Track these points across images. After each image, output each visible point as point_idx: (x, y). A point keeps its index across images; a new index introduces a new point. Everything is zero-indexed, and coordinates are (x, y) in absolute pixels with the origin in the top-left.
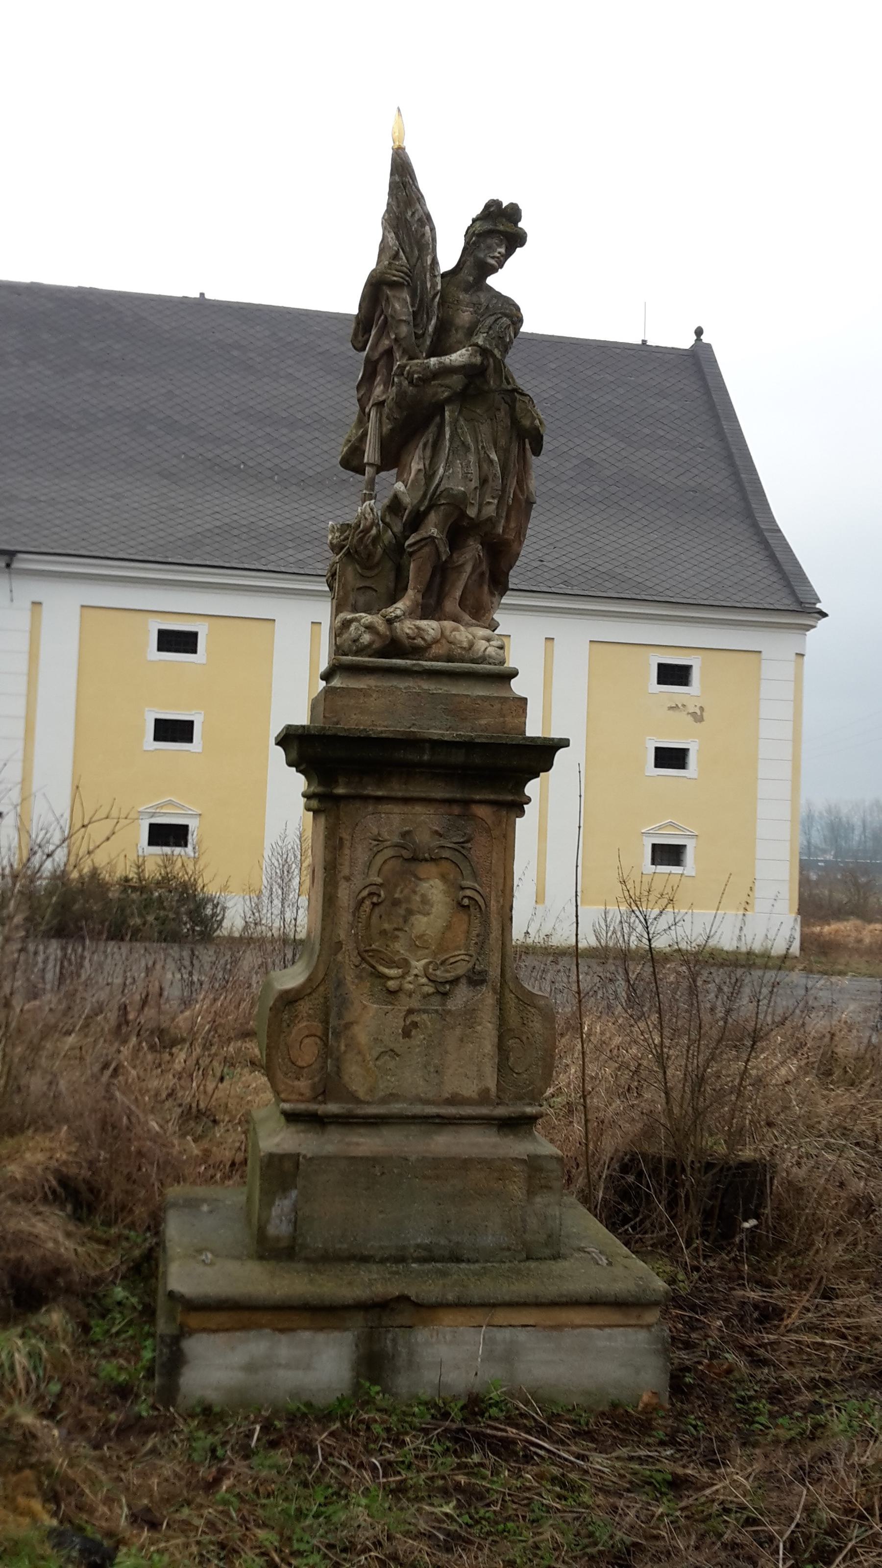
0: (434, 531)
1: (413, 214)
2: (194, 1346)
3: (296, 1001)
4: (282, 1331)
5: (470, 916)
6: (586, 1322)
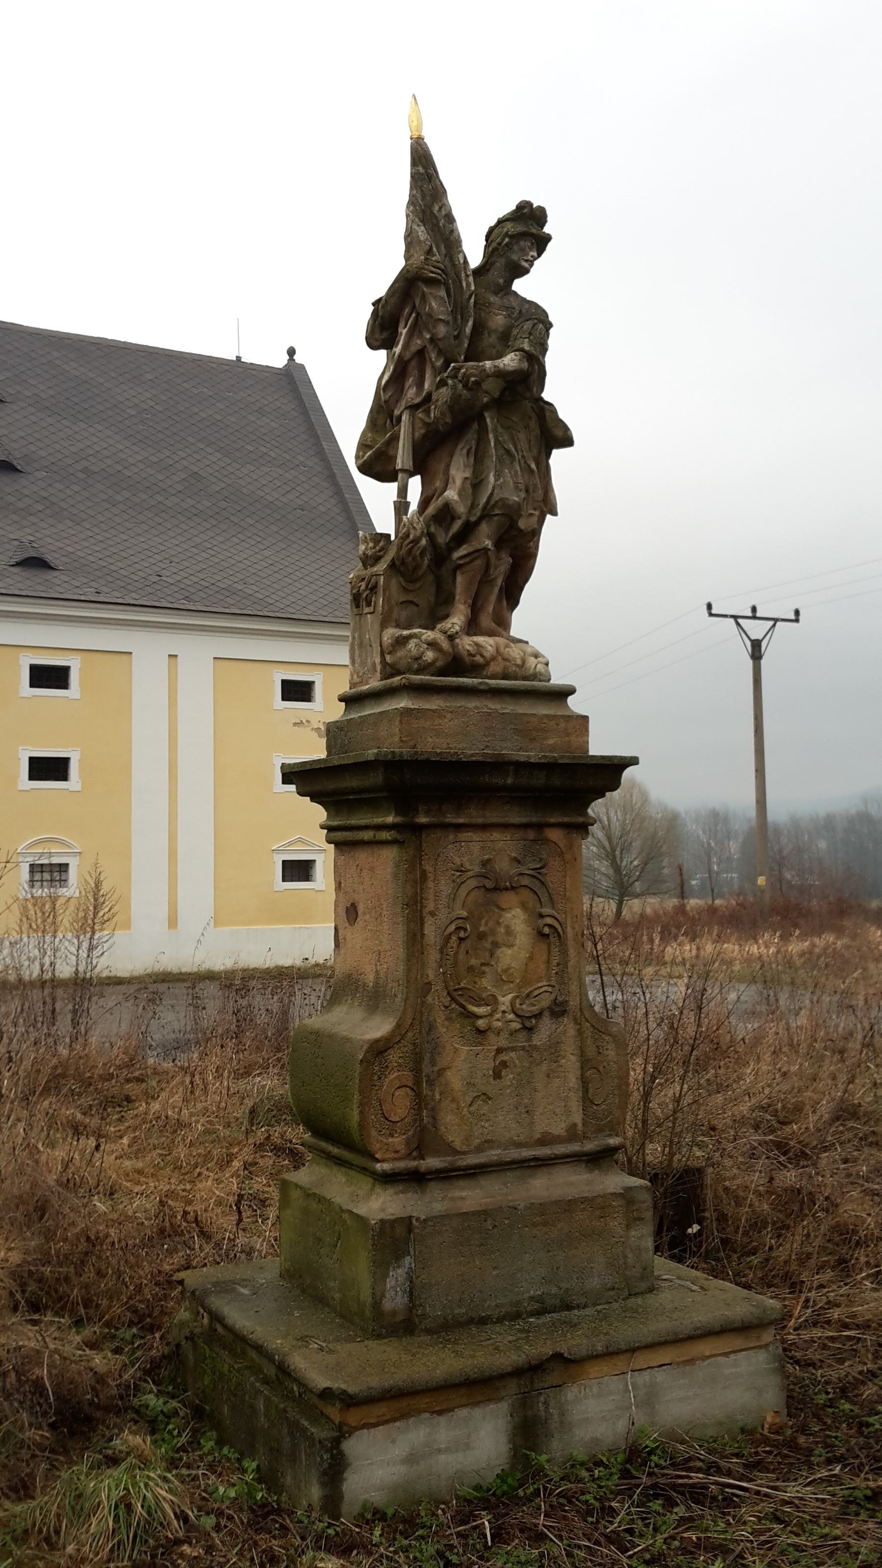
0: (488, 543)
1: (440, 208)
2: (352, 1446)
3: (386, 1051)
4: (440, 1413)
5: (549, 945)
6: (714, 1352)
